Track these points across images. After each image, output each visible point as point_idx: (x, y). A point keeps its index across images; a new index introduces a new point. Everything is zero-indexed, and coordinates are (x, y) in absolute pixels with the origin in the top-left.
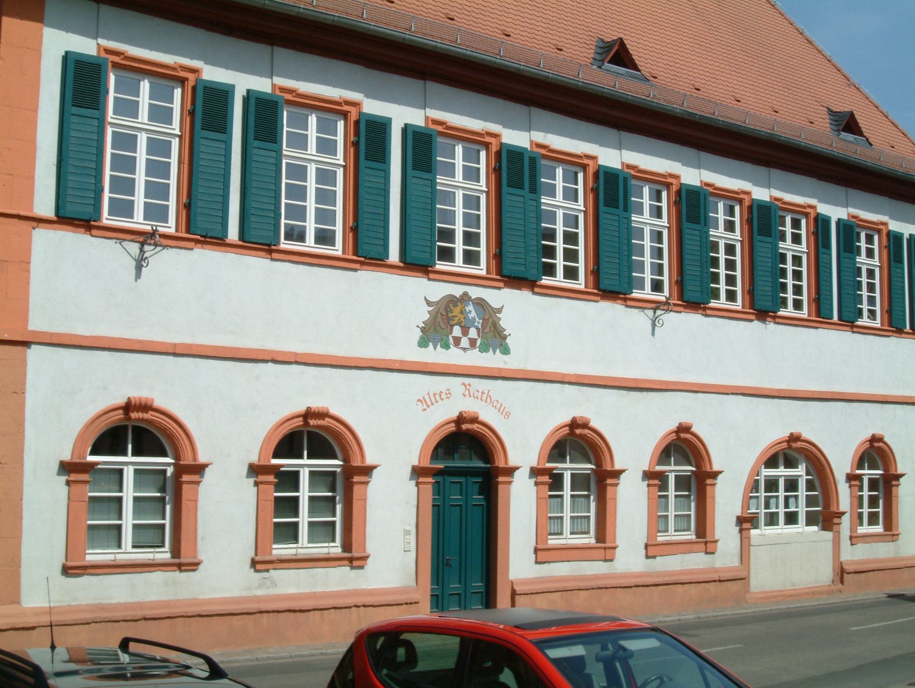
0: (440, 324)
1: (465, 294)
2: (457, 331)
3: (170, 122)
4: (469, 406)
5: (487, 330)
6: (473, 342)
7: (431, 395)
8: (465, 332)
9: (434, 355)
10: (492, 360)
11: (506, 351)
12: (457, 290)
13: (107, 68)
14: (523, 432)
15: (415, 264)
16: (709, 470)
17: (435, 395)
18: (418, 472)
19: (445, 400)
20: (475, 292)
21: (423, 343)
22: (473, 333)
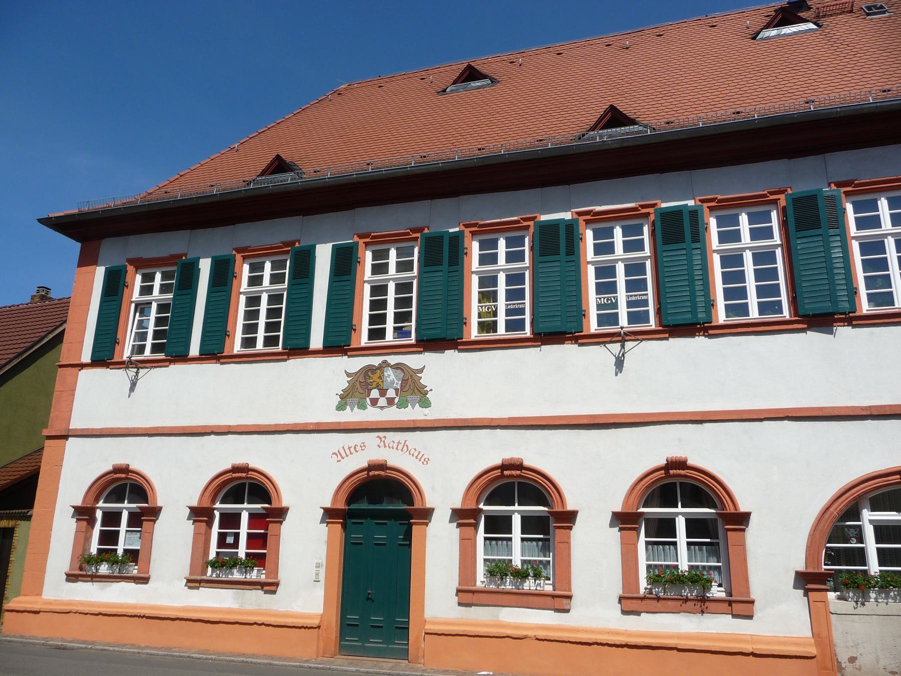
0: (361, 388)
1: (385, 362)
2: (375, 393)
3: (771, 236)
6: (390, 402)
8: (383, 393)
9: (352, 415)
10: (413, 413)
11: (425, 404)
12: (376, 361)
13: (703, 213)
14: (444, 474)
15: (337, 344)
16: (733, 511)
17: (349, 448)
18: (330, 514)
19: (360, 452)
20: (393, 360)
21: (340, 407)
22: (391, 393)
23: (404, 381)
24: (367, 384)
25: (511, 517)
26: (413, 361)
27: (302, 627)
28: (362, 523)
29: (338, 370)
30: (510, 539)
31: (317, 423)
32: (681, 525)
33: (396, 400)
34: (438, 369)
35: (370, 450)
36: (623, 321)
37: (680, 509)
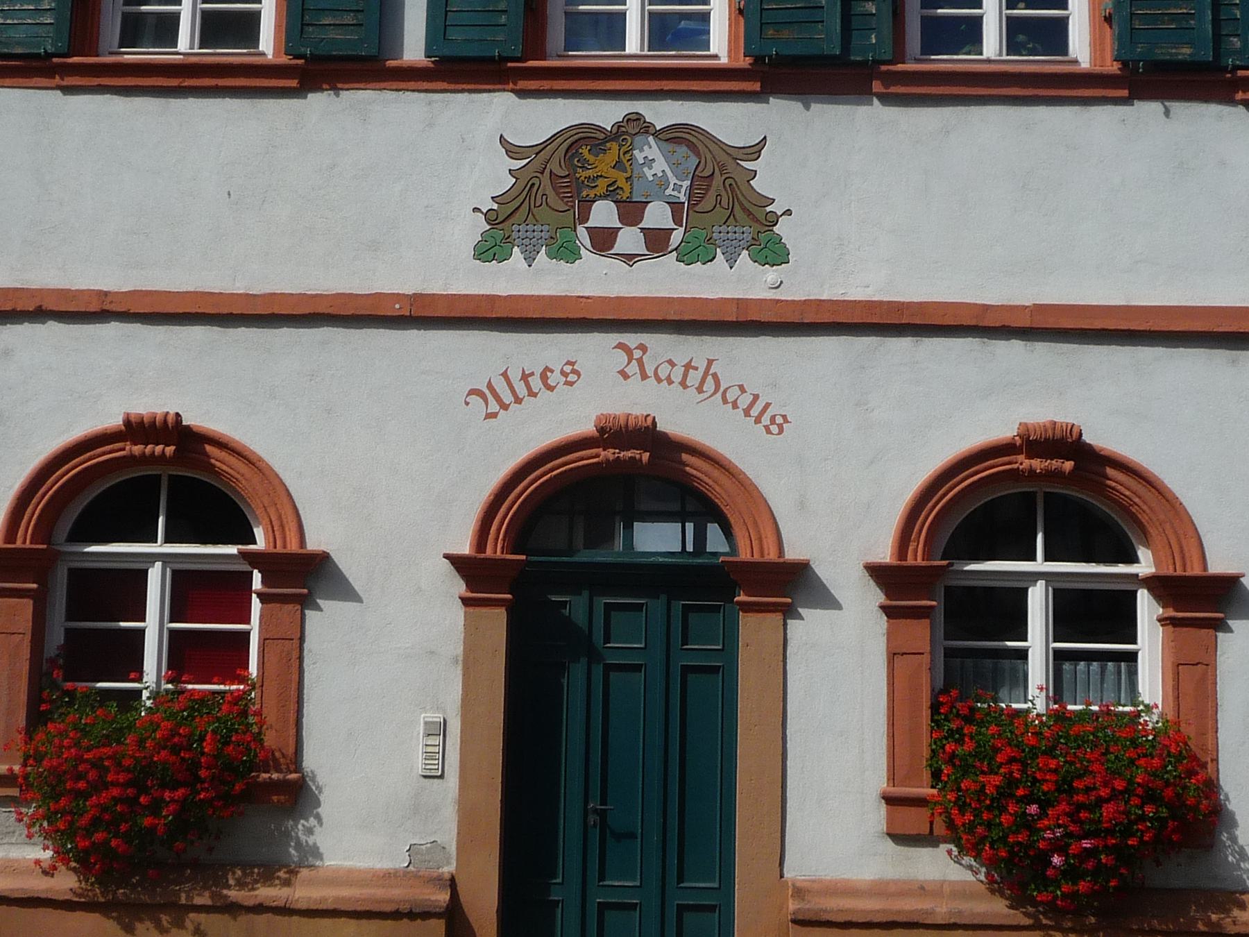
0: (551, 196)
1: (635, 118)
2: (604, 214)
4: (635, 400)
5: (708, 204)
7: (515, 376)
8: (631, 212)
10: (732, 279)
11: (772, 252)
12: (606, 113)
14: (836, 466)
17: (525, 377)
20: (662, 113)
22: (657, 215)
23: (700, 183)
24: (579, 185)
25: (144, 573)
26: (727, 121)
27: (396, 915)
28: (639, 607)
29: (483, 136)
30: (1132, 657)
31: (417, 297)
32: (1037, 601)
33: (677, 237)
34: (809, 152)
35: (588, 391)
36: (634, 41)
37: (1039, 565)
